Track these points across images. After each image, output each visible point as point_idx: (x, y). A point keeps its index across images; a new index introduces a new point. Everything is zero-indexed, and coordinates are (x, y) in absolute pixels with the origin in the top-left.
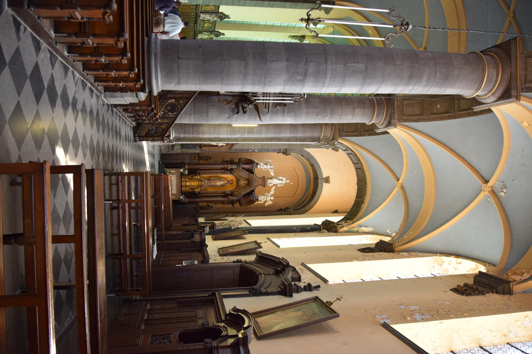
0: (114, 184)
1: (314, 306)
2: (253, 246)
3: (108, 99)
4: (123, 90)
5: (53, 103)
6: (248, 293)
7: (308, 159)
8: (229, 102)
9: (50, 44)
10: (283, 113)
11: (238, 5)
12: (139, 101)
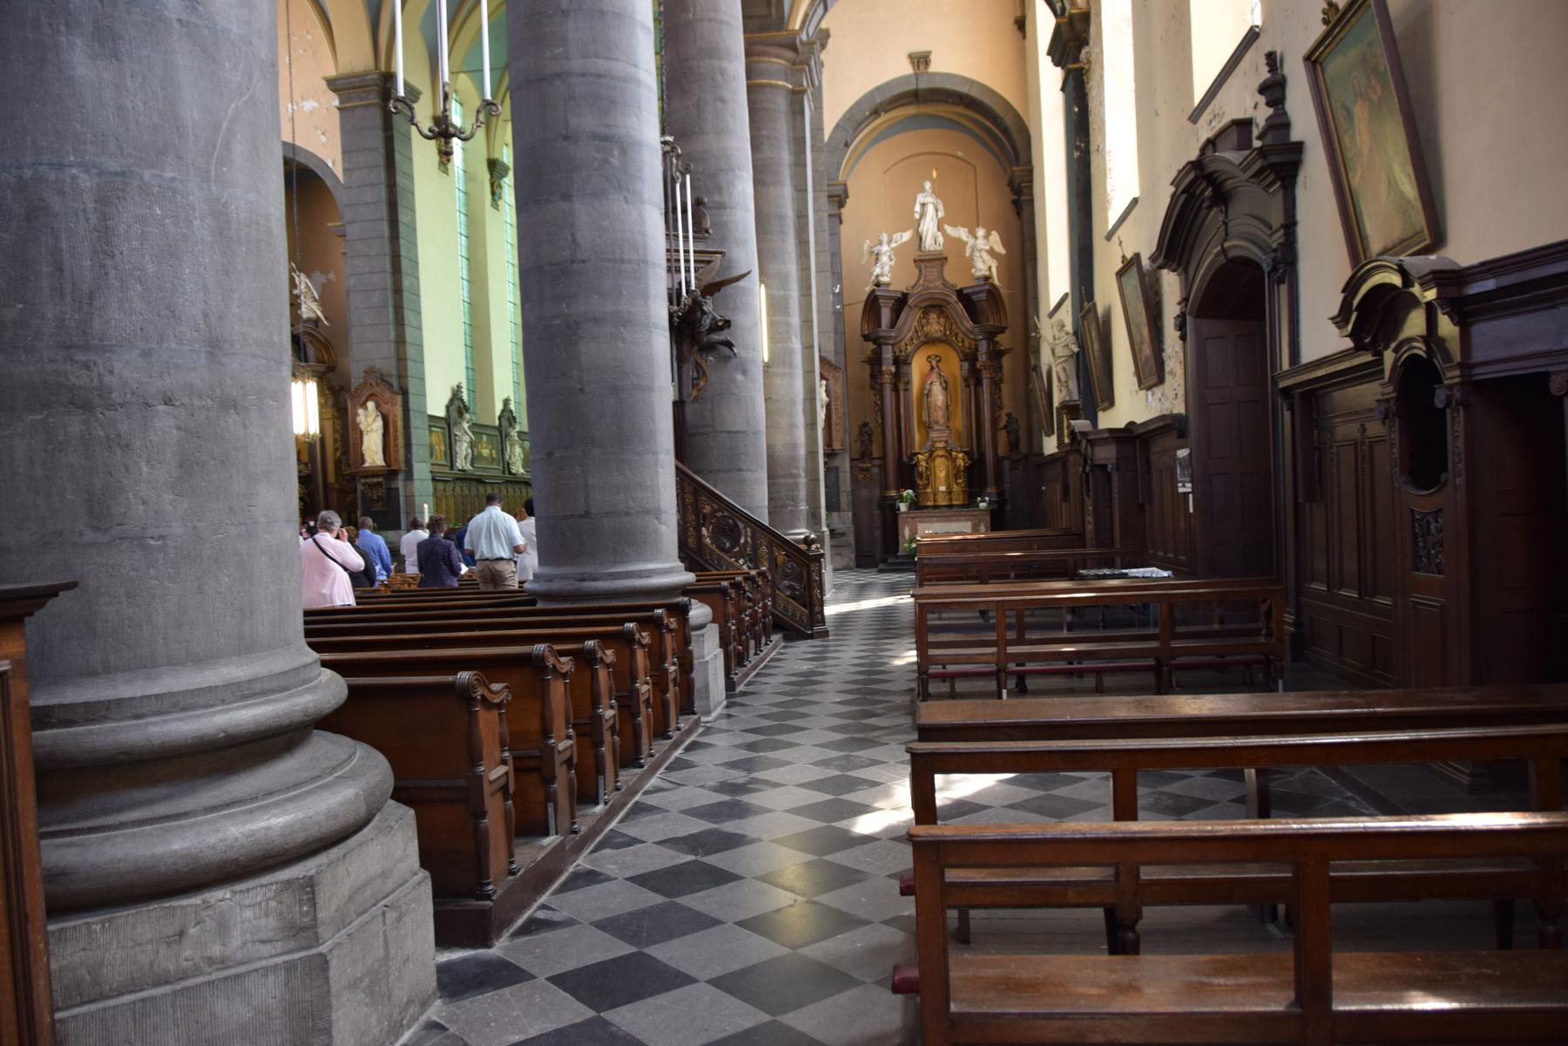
0: (952, 687)
1: (1336, 65)
2: (1132, 280)
3: (712, 704)
4: (686, 664)
5: (735, 841)
6: (1284, 288)
7: (858, 128)
8: (701, 372)
9: (578, 849)
10: (722, 207)
11: (422, 363)
12: (713, 621)
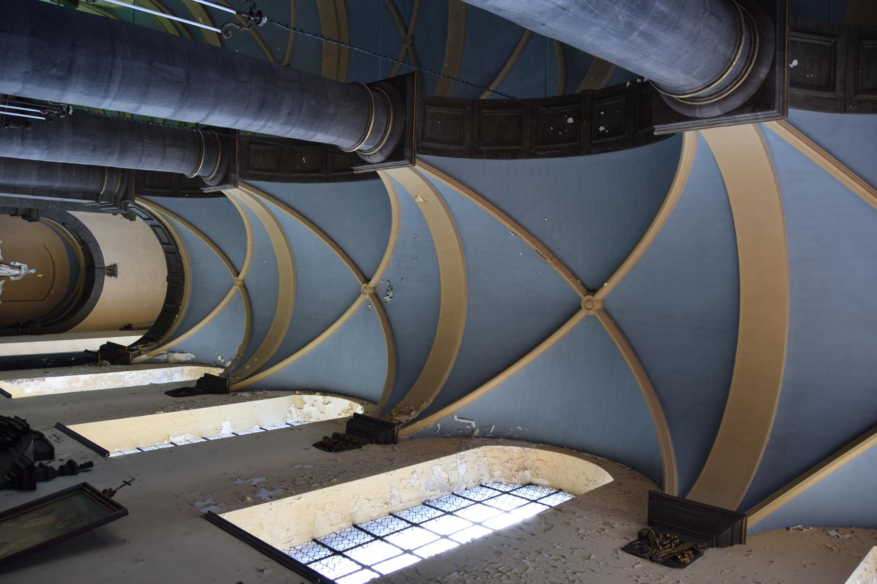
1: (79, 501)
10: (24, 138)
